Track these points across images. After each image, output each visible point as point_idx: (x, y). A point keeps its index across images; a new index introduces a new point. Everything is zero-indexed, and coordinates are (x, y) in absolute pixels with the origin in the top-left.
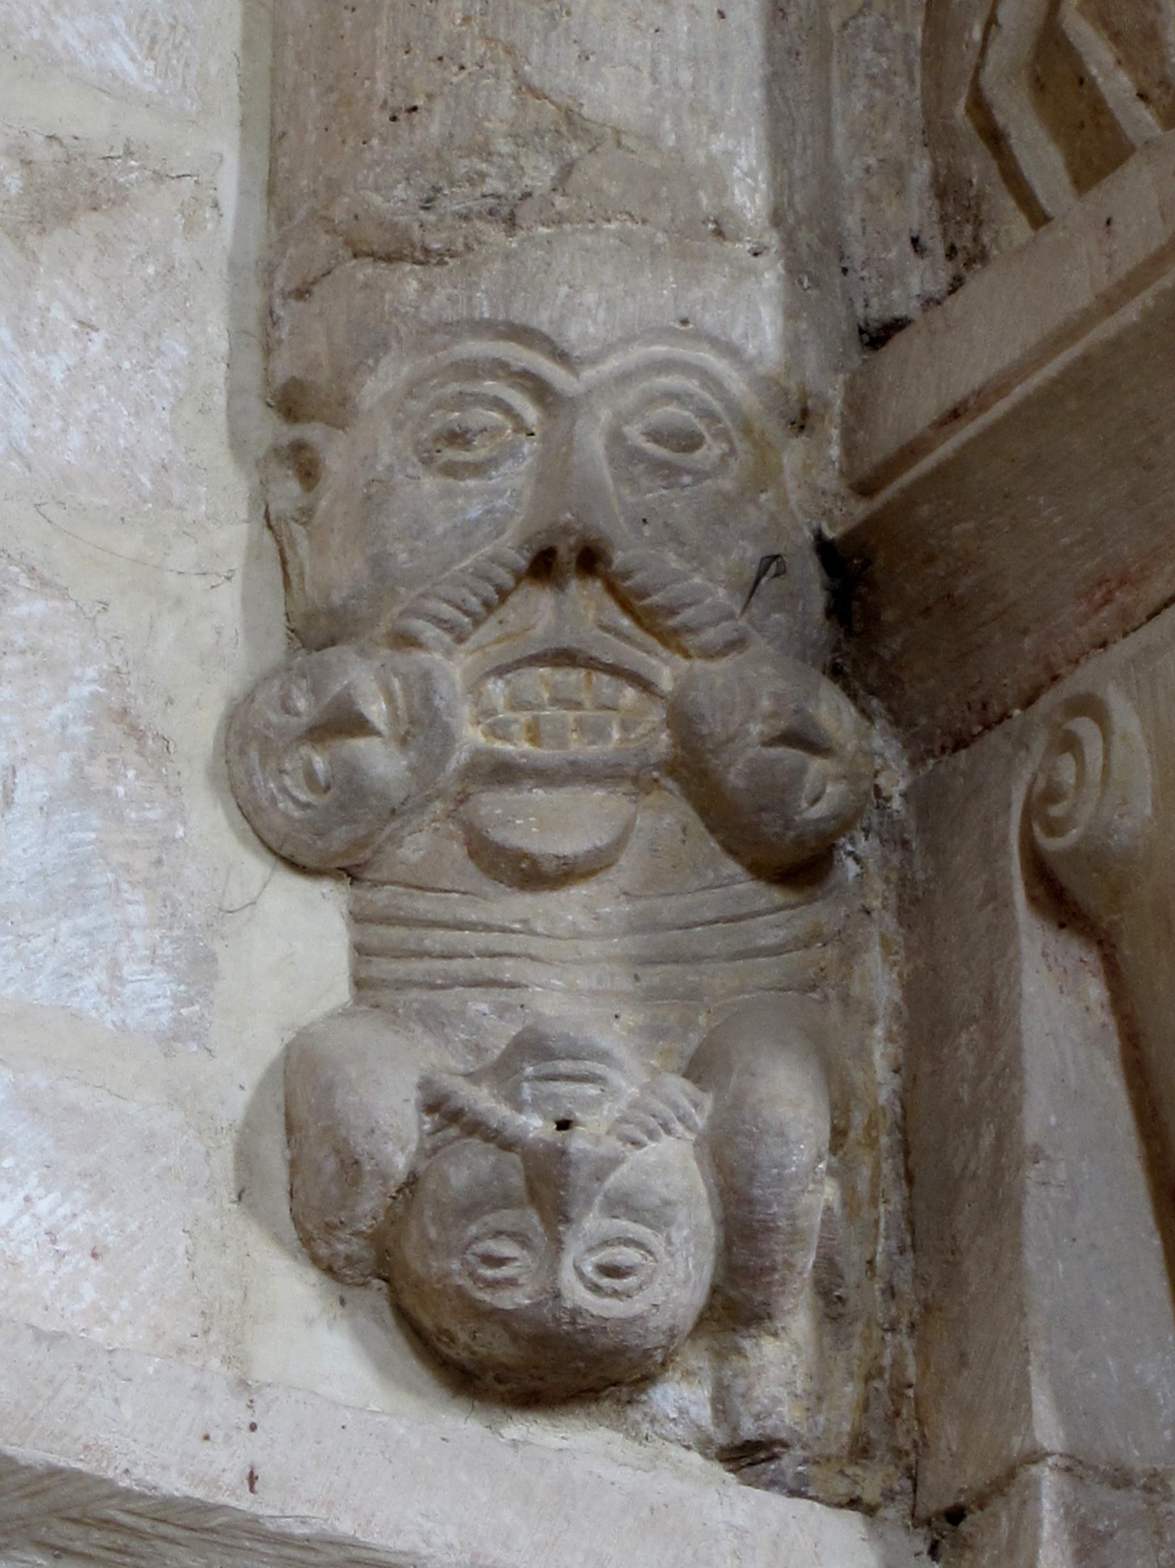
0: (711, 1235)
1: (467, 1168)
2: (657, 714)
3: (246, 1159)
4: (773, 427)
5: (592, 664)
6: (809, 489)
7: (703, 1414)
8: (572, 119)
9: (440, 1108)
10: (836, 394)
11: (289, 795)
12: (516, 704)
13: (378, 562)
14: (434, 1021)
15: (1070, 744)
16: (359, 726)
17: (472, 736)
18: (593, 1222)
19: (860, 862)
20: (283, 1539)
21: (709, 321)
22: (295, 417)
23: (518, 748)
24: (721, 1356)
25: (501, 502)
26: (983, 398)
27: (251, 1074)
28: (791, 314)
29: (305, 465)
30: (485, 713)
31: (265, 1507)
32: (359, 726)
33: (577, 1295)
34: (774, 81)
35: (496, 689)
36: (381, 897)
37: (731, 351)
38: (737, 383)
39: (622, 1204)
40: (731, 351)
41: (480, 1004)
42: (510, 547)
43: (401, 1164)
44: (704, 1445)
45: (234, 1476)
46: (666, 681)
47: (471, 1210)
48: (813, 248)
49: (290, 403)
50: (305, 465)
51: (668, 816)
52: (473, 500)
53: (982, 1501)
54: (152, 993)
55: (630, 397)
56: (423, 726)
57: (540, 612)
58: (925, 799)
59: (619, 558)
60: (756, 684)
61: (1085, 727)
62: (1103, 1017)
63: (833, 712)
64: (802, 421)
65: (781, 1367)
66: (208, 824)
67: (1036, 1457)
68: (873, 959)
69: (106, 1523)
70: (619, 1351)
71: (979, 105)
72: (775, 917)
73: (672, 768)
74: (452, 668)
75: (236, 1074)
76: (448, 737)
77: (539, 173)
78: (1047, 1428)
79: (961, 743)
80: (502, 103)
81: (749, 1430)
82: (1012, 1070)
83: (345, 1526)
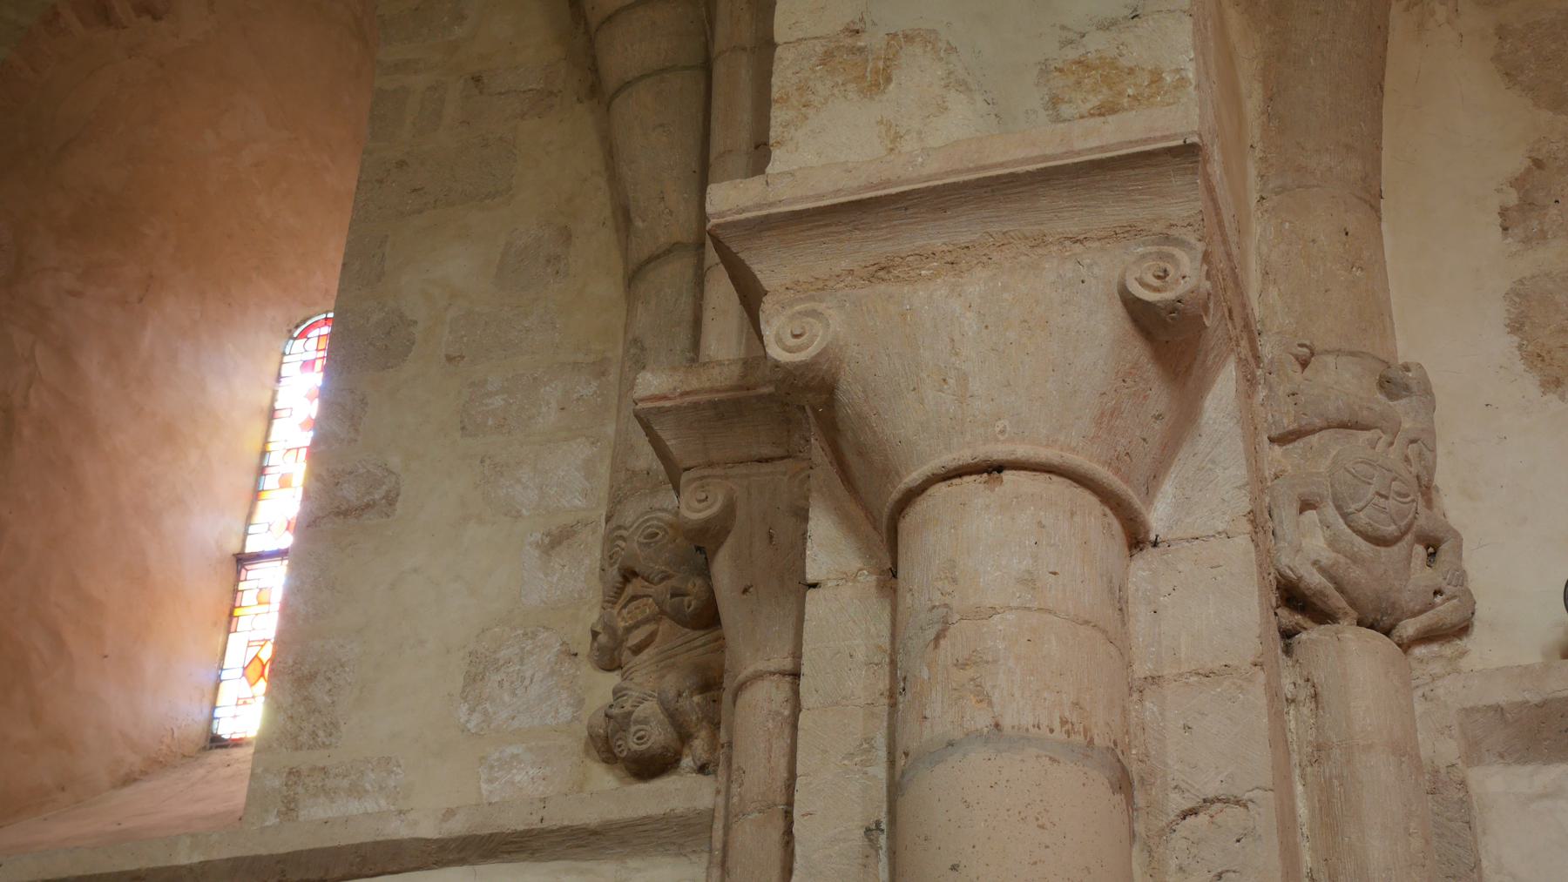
33: (636, 747)
35: (625, 612)
39: (637, 722)
51: (665, 625)
57: (630, 590)
83: (566, 823)
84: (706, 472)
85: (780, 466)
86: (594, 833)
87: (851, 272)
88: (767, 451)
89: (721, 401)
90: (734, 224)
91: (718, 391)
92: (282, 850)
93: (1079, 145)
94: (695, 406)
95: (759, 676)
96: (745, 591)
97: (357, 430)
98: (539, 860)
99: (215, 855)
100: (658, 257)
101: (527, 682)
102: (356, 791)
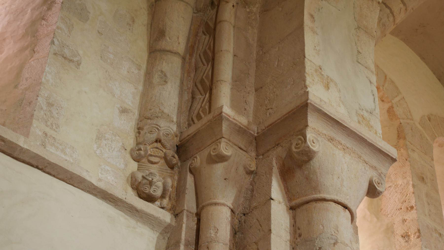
0: (162, 190)
1: (145, 181)
2: (163, 153)
3: (128, 179)
4: (174, 136)
5: (159, 149)
6: (176, 141)
7: (159, 205)
8: (163, 112)
9: (143, 177)
10: (179, 135)
11: (135, 154)
12: (153, 151)
13: (144, 139)
14: (143, 172)
15: (194, 160)
16: (141, 150)
17: (149, 152)
18: (154, 187)
19: (176, 169)
20: (127, 203)
21: (171, 127)
22: (139, 129)
23: (153, 154)
24: (161, 200)
25: (154, 136)
26: (190, 134)
27: (129, 174)
28: (177, 129)
29: (139, 133)
30: (150, 151)
31: (126, 200)
32: (141, 150)
33: (152, 192)
34: (177, 113)
35: (152, 150)
36: (140, 164)
37: (172, 130)
38: (172, 132)
39: (156, 186)
40: (172, 130)
41: (147, 171)
42: (154, 140)
43: (140, 180)
44: (159, 207)
45: (124, 198)
46: (164, 151)
47: (144, 185)
48: (179, 126)
49: (139, 129)
50: (139, 133)
51: (163, 161)
52: (152, 136)
53: (180, 213)
54: (122, 166)
55: (165, 131)
56: (146, 151)
57: (156, 145)
58: (181, 166)
59: (162, 141)
60: (171, 153)
61: (195, 159)
62: (193, 180)
63: (176, 156)
64: (176, 136)
65: (165, 202)
66: (128, 156)
67: (184, 210)
68: (176, 176)
69: (114, 199)
70: (154, 197)
71: (192, 119)
72: (169, 171)
73: (164, 158)
74: (149, 147)
75: (128, 173)
76: (147, 152)
77: (160, 115)
78: (186, 208)
79: (185, 161)
80: (158, 110)
81: (162, 206)
82: (186, 183)
83: (132, 203)
84: (228, 142)
85: (244, 153)
86: (137, 210)
87: (325, 135)
88: (242, 147)
89: (242, 128)
90: (313, 106)
91: (241, 124)
92: (52, 161)
93: (378, 143)
94: (236, 125)
95: (224, 205)
96: (225, 179)
97: (70, 34)
98: (115, 208)
99: (32, 149)
100: (172, 52)
101: (113, 149)
102: (63, 151)
